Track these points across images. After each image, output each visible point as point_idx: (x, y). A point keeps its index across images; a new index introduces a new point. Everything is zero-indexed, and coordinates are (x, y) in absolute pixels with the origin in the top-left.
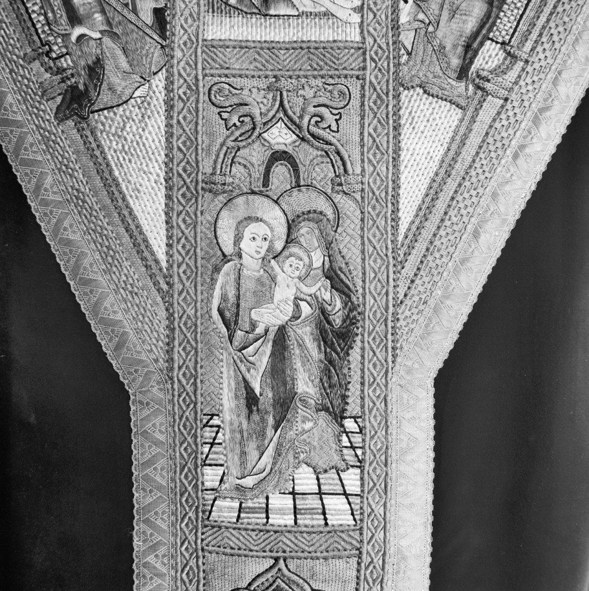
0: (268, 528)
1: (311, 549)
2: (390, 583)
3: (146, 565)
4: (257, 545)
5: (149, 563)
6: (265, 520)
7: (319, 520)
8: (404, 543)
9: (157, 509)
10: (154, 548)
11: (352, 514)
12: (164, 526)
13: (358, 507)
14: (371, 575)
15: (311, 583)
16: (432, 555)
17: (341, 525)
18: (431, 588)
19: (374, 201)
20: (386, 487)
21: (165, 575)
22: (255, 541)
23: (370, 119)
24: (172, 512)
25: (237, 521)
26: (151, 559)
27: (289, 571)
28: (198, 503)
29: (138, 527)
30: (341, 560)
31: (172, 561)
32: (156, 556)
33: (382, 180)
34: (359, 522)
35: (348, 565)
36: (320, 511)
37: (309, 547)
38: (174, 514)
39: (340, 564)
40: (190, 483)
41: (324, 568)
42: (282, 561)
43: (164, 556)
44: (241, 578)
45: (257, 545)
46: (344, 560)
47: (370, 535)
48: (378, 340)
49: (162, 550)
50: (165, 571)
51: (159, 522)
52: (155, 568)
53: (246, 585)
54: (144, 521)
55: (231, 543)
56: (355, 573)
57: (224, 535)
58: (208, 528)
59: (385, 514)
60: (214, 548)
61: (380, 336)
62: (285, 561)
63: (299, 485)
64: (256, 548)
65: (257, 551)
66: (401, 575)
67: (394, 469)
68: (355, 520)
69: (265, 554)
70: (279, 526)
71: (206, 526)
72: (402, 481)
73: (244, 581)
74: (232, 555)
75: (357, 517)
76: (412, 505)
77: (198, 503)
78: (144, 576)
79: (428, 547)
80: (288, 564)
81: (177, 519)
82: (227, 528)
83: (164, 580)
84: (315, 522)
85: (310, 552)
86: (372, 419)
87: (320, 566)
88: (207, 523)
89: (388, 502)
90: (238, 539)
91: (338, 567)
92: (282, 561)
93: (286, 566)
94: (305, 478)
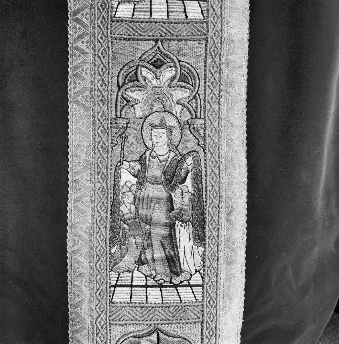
0: (151, 20)
1: (177, 34)
2: (224, 57)
3: (76, 48)
4: (145, 32)
5: (78, 46)
6: (149, 17)
7: (182, 16)
8: (233, 31)
9: (83, 12)
10: (81, 37)
11: (202, 13)
12: (87, 22)
13: (205, 9)
14: (210, 333)
15: (178, 57)
16: (249, 40)
17: (195, 19)
18: (240, 343)
19: (214, 15)
20: (218, 250)
21: (88, 53)
22: (143, 29)
23: (211, 45)
24: (92, 13)
25: (133, 16)
26: (79, 44)
27: (164, 48)
28: (108, 6)
29: (71, 24)
30: (195, 42)
31: (92, 45)
32: (83, 42)
33: (219, 33)
34: (206, 18)
35: (200, 45)
36: (183, 10)
37: (176, 32)
38: (93, 14)
39: (195, 44)
40: (103, 26)
41: (186, 47)
42: (159, 43)
43: (87, 42)
44: (135, 54)
45: (145, 32)
46: (197, 41)
47: (208, 310)
48: (213, 271)
49: (86, 38)
50: (87, 51)
51: (84, 20)
52: (82, 49)
53: (138, 58)
54: (75, 20)
55: (129, 32)
56: (204, 50)
57: (124, 26)
58: (114, 23)
59: (221, 13)
60: (118, 36)
61: (214, 269)
62: (162, 42)
63: (170, 8)
64: (144, 34)
65: (145, 36)
66: (231, 51)
67: (220, 323)
68: (203, 16)
69: (150, 38)
70: (158, 19)
71: (113, 21)
72: (225, 327)
73: (137, 55)
74: (129, 40)
75: (205, 15)
76: (236, 9)
77: (108, 6)
78: (75, 55)
79: (247, 35)
80: (164, 45)
81: (95, 17)
82: (126, 21)
83: (87, 57)
84: (180, 18)
85: (177, 36)
86: (210, 226)
87: (182, 45)
88: (114, 19)
89: (223, 5)
90: (133, 29)
91: (193, 46)
92: (159, 43)
93: (162, 46)
94: (173, 8)
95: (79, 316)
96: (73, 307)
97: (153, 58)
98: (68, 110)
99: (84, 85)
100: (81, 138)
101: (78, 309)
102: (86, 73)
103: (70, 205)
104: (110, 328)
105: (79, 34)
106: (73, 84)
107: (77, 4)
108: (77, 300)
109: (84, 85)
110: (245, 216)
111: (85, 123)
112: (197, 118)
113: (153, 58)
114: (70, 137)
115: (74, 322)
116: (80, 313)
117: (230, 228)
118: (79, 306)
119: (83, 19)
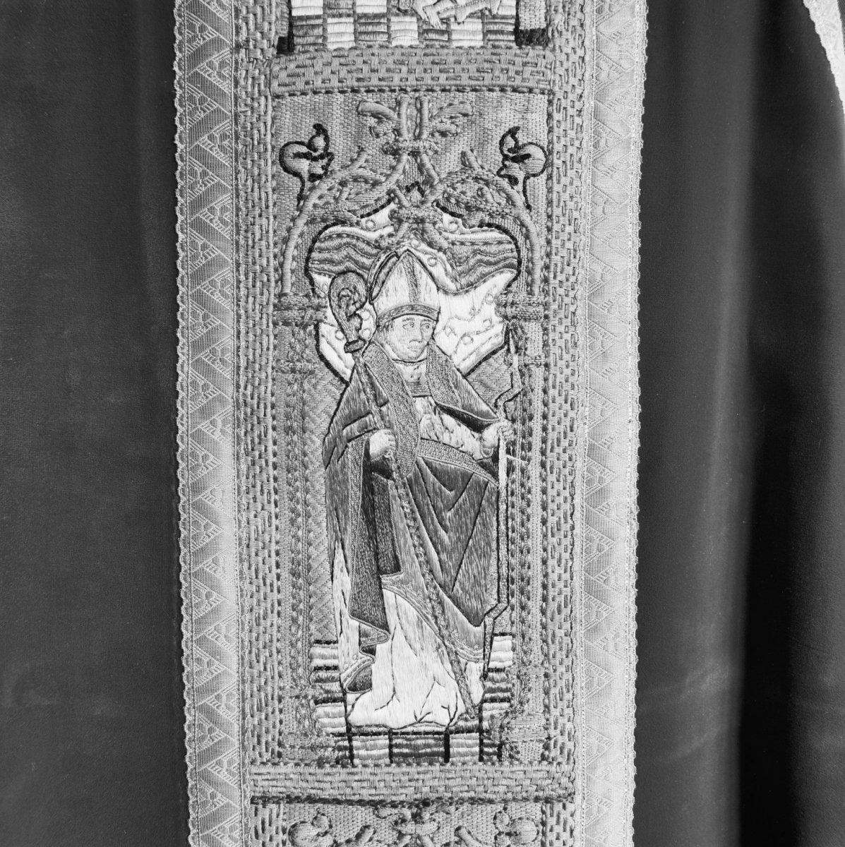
51: (214, 79)
95: (209, 713)
96: (197, 488)
97: (376, 795)
98: (175, 386)
99: (217, 179)
100: (214, 667)
101: (206, 564)
102: (220, 75)
103: (184, 482)
104: (281, 706)
105: (204, 262)
106: (187, 102)
107: (199, 394)
108: (202, 472)
109: (217, 179)
110: (631, 554)
111: (217, 64)
112: (530, 285)
113: (376, 795)
114: (182, 439)
115: (199, 734)
116: (209, 294)
117: (595, 537)
118: (213, 691)
119: (214, 221)
